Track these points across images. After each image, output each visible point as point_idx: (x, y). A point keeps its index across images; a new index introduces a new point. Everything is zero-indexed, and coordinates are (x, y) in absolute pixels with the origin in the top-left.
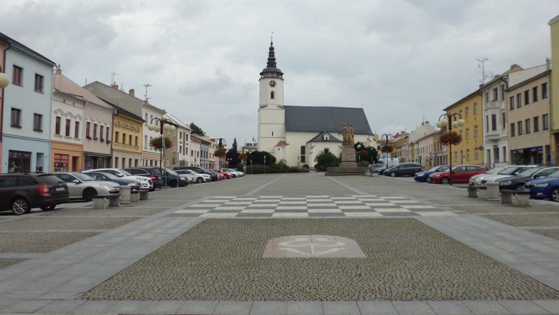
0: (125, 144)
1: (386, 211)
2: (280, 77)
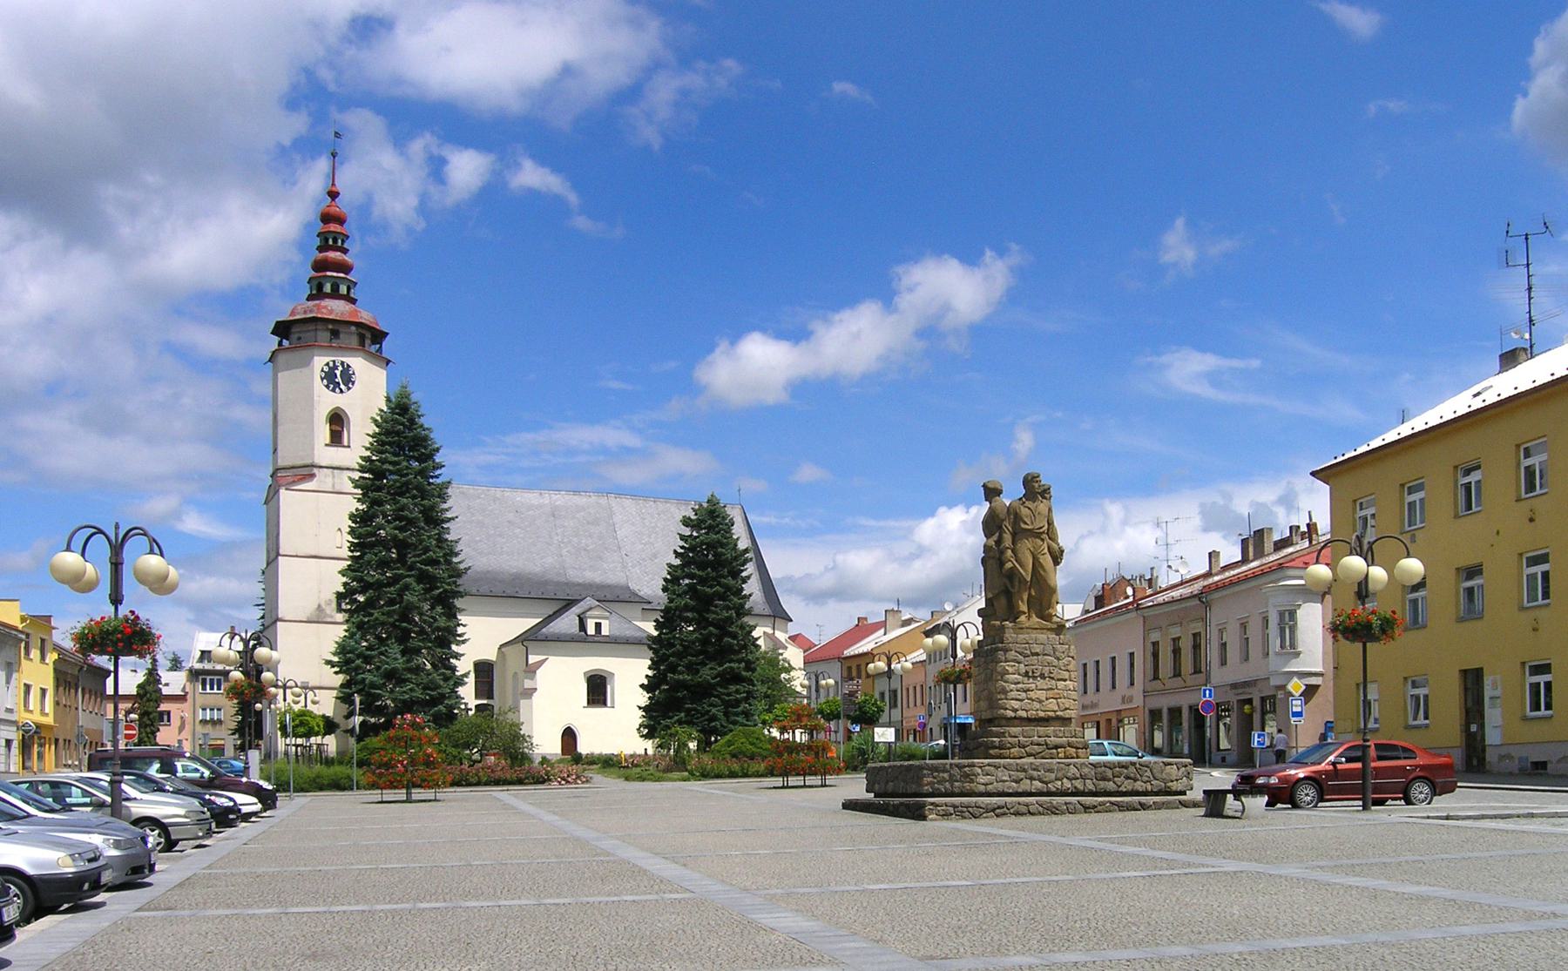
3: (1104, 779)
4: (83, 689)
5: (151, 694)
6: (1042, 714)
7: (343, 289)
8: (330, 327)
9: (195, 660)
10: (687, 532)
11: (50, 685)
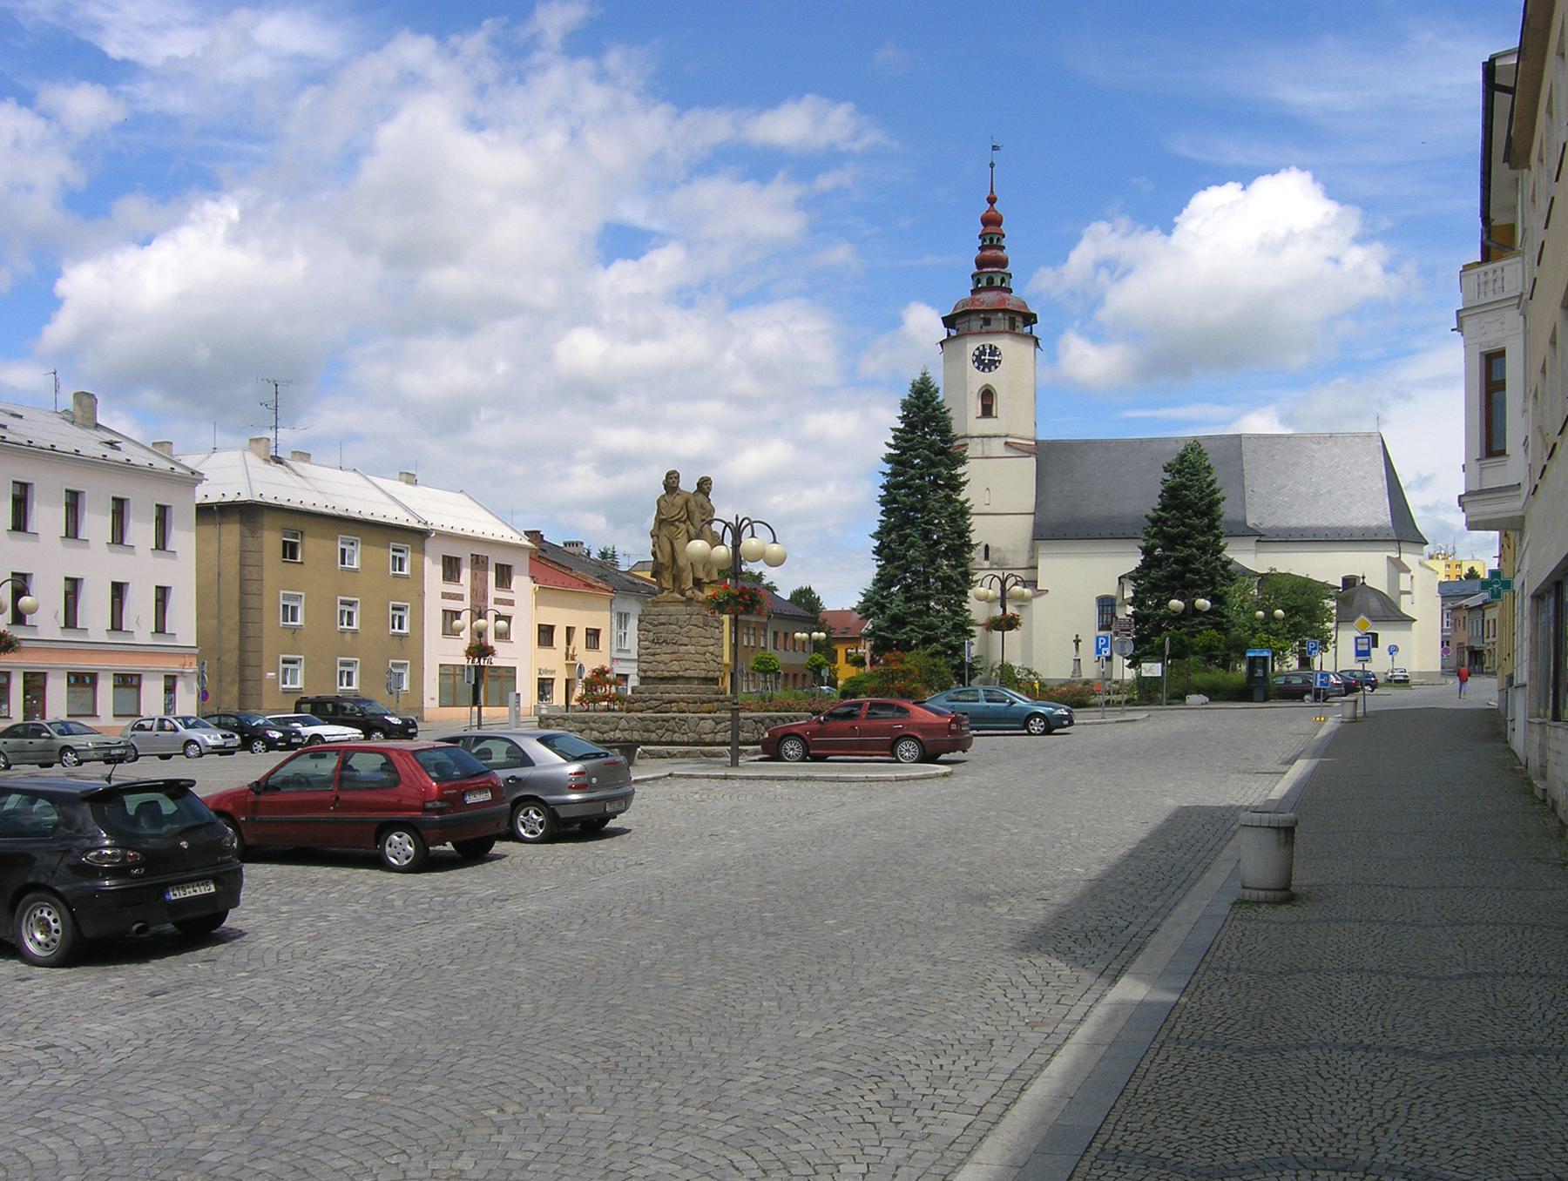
0: (1043, 548)
1: (1103, 860)
2: (1027, 329)
3: (647, 731)
6: (666, 674)
7: (997, 282)
8: (982, 316)
10: (1167, 476)
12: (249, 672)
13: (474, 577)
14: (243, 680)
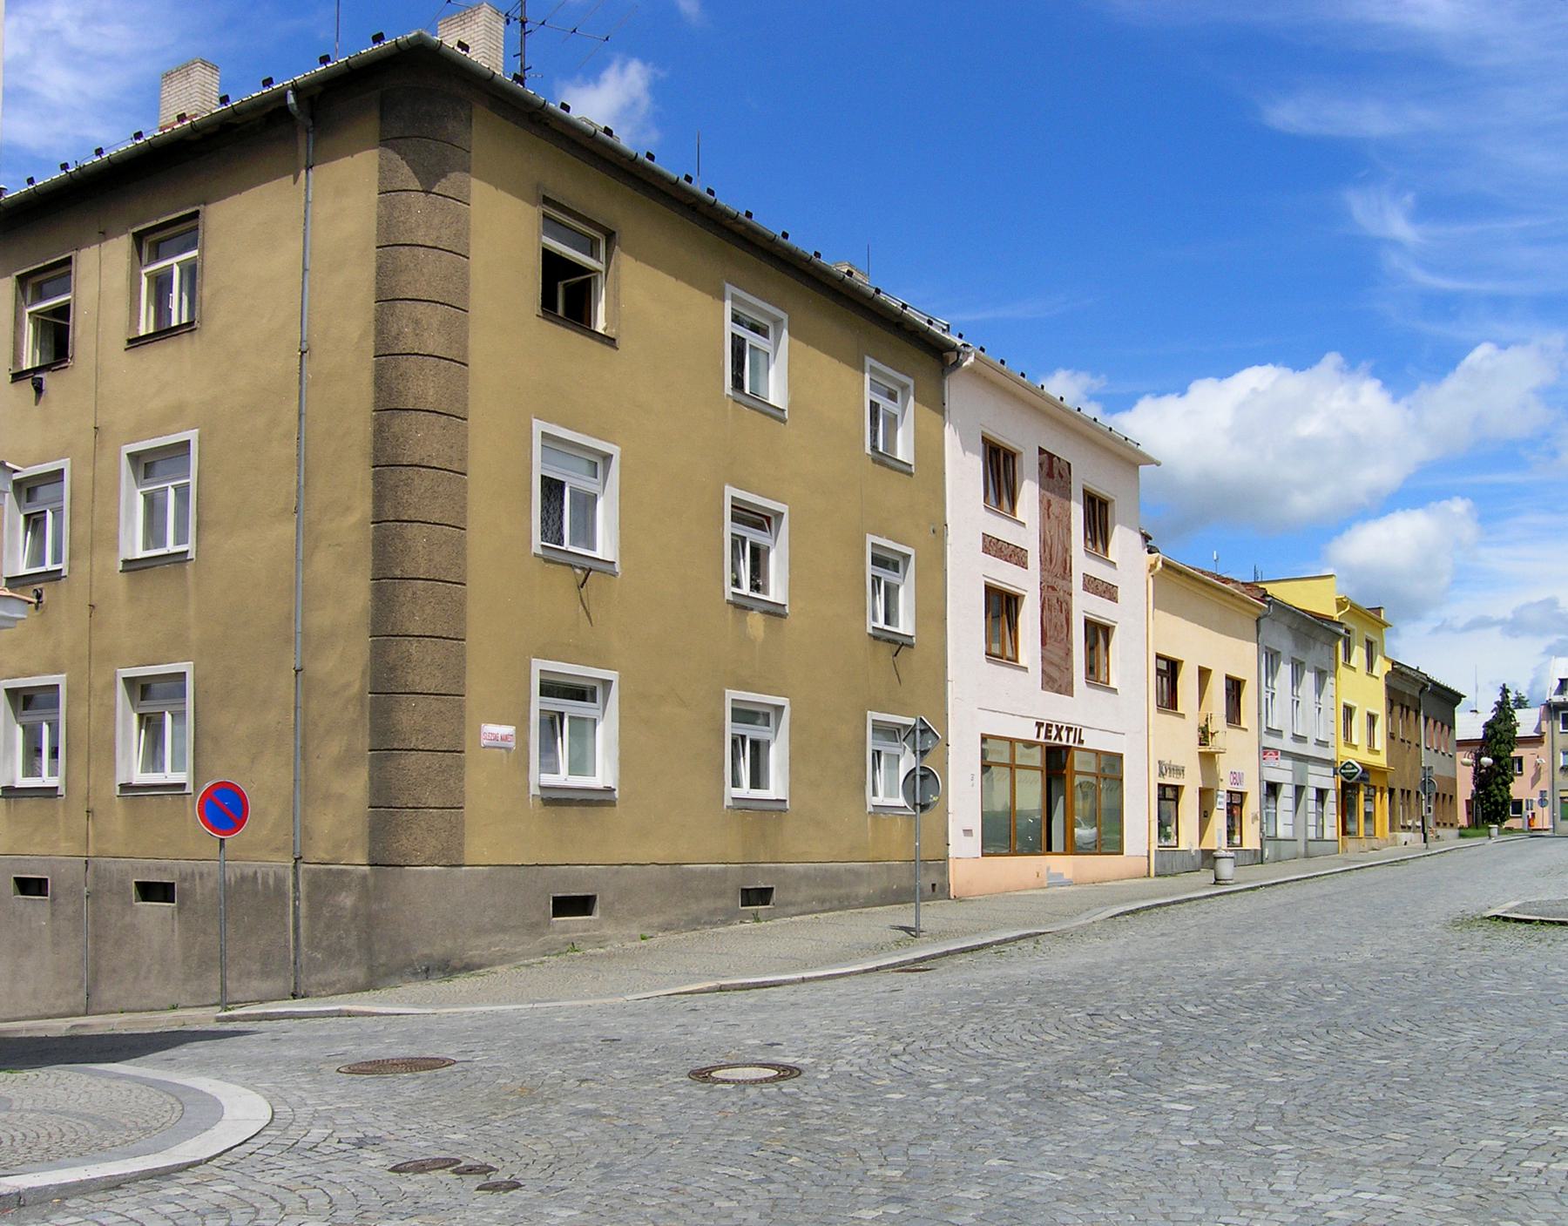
4: (1426, 719)
5: (1502, 735)
9: (1553, 692)
11: (1380, 707)
12: (410, 717)
13: (1046, 507)
14: (385, 749)
